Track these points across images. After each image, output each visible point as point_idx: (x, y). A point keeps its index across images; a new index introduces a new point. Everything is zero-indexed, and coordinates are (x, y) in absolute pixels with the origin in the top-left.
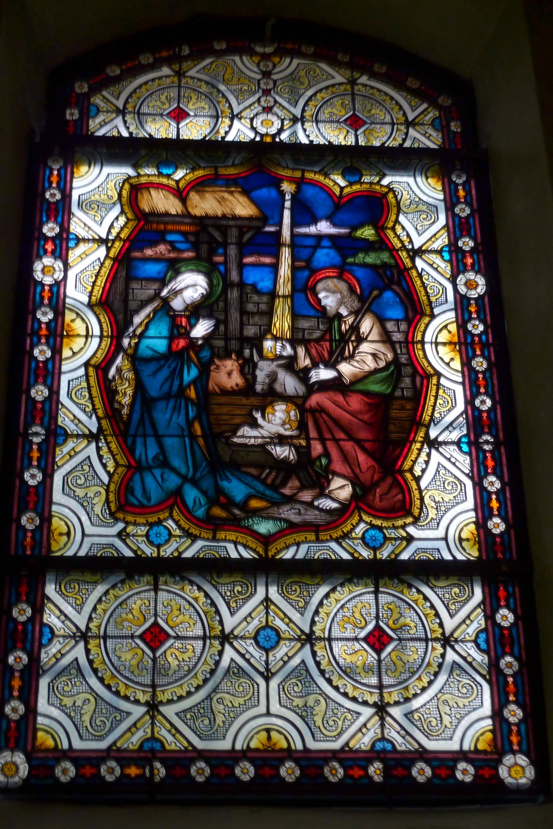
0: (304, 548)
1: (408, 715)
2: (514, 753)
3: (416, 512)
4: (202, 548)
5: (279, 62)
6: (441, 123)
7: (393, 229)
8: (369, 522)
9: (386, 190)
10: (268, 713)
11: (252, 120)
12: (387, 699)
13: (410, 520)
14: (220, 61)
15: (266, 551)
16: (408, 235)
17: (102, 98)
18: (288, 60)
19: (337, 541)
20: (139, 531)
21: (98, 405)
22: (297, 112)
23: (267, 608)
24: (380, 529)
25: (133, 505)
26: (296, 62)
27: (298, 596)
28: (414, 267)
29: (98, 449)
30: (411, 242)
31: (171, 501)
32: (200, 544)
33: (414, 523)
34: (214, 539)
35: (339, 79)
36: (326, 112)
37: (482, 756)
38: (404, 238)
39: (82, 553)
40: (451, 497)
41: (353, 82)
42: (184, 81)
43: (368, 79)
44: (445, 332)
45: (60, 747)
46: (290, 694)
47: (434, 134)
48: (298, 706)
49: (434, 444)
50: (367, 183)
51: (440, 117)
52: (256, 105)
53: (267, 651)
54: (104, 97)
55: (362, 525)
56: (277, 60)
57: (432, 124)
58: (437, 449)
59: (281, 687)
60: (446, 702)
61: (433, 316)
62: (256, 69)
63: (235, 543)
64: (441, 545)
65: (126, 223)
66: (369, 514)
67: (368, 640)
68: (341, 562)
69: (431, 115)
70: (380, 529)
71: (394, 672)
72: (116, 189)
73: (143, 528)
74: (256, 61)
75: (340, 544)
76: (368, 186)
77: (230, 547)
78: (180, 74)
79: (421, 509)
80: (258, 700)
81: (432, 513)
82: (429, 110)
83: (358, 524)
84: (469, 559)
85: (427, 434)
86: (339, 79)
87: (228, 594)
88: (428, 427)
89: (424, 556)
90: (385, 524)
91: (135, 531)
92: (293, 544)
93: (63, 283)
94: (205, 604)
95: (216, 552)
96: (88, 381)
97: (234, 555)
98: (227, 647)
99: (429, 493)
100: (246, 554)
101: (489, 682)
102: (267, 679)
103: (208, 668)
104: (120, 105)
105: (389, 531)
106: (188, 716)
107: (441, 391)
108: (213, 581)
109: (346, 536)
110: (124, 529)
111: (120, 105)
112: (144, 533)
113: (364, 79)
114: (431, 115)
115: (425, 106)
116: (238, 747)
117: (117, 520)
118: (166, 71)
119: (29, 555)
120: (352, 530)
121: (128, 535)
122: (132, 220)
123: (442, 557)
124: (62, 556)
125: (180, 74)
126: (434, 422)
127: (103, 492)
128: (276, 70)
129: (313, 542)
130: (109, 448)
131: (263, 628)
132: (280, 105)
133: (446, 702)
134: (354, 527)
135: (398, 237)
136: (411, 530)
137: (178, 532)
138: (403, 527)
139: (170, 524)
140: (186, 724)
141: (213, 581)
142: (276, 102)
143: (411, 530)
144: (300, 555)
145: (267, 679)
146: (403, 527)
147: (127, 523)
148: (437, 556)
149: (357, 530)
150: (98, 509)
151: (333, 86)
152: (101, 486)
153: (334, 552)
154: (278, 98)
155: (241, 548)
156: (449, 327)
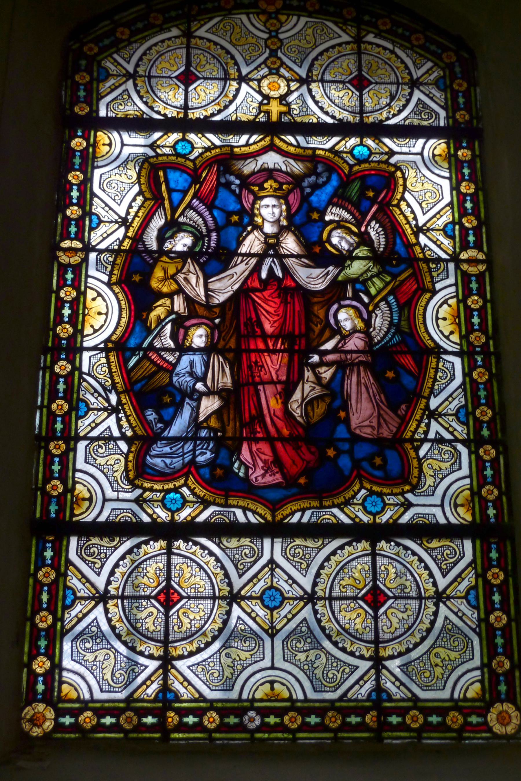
0: (308, 513)
1: (404, 667)
2: (502, 702)
3: (415, 481)
4: (414, 516)
5: (286, 21)
6: (445, 83)
7: (398, 206)
8: (369, 488)
9: (136, 482)
10: (273, 667)
11: (259, 81)
12: (382, 653)
13: (407, 488)
14: (227, 21)
15: (274, 516)
16: (413, 212)
17: (113, 61)
18: (295, 18)
19: (338, 506)
20: (155, 497)
21: (118, 379)
22: (303, 72)
23: (272, 570)
24: (380, 495)
25: (148, 474)
26: (303, 20)
27: (301, 558)
28: (418, 243)
29: (119, 420)
30: (415, 218)
31: (185, 470)
32: (212, 509)
33: (411, 491)
34: (227, 505)
35: (346, 38)
36: (332, 72)
37: (469, 704)
38: (408, 214)
39: (102, 519)
40: (448, 465)
41: (358, 40)
42: (193, 41)
43: (375, 37)
44: (445, 306)
45: (82, 697)
46: (292, 648)
47: (438, 94)
48: (300, 660)
49: (434, 415)
50: (375, 162)
51: (444, 77)
52: (263, 66)
53: (272, 610)
54: (115, 60)
55: (363, 491)
56: (283, 18)
57: (436, 83)
58: (436, 420)
59: (285, 643)
60: (308, 42)
61: (434, 292)
62: (262, 28)
63: (245, 509)
64: (438, 511)
65: (143, 203)
66: (371, 482)
67: (366, 598)
68: (342, 525)
69: (435, 74)
70: (380, 495)
71: (390, 628)
72: (425, 476)
73: (158, 494)
74: (263, 20)
75: (342, 510)
76: (376, 165)
77: (239, 513)
78: (188, 35)
79: (419, 478)
80: (264, 655)
81: (430, 481)
82: (434, 70)
83: (359, 491)
84: (462, 524)
85: (127, 231)
86: (346, 38)
87: (237, 556)
88: (428, 399)
89: (420, 521)
90: (385, 490)
91: (151, 496)
92: (298, 510)
93: (84, 265)
94: (222, 582)
95: (226, 516)
96: (432, 277)
97: (299, 138)
98: (235, 606)
99: (428, 462)
100: (253, 519)
101: (479, 635)
102: (272, 636)
103: (216, 626)
104: (131, 69)
105: (388, 497)
106: (200, 670)
107: (441, 364)
108: (221, 545)
109: (347, 503)
110: (141, 495)
111: (131, 69)
112: (160, 498)
113: (370, 38)
114: (435, 74)
115: (429, 64)
116: (245, 696)
117: (135, 487)
118: (175, 32)
119: (53, 518)
120: (354, 497)
121: (145, 501)
122: (149, 199)
123: (437, 520)
124: (78, 521)
125: (188, 35)
126: (434, 393)
127: (123, 460)
128: (283, 29)
129: (317, 508)
130: (128, 421)
131: (276, 608)
132: (287, 66)
133: (437, 655)
134: (356, 493)
135: (402, 213)
136: (409, 496)
137: (191, 498)
138: (402, 494)
139: (185, 490)
140: (197, 676)
141: (221, 545)
142: (283, 63)
143: (409, 496)
144: (305, 520)
145: (272, 636)
146: (402, 494)
147: (145, 490)
148: (433, 521)
149: (359, 496)
150: (117, 475)
151: (340, 45)
152: (121, 455)
153: (335, 516)
154: (285, 59)
155: (250, 514)
156: (450, 302)
